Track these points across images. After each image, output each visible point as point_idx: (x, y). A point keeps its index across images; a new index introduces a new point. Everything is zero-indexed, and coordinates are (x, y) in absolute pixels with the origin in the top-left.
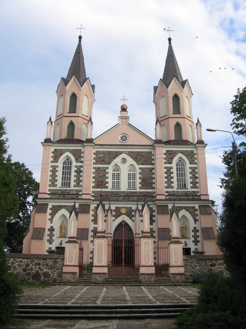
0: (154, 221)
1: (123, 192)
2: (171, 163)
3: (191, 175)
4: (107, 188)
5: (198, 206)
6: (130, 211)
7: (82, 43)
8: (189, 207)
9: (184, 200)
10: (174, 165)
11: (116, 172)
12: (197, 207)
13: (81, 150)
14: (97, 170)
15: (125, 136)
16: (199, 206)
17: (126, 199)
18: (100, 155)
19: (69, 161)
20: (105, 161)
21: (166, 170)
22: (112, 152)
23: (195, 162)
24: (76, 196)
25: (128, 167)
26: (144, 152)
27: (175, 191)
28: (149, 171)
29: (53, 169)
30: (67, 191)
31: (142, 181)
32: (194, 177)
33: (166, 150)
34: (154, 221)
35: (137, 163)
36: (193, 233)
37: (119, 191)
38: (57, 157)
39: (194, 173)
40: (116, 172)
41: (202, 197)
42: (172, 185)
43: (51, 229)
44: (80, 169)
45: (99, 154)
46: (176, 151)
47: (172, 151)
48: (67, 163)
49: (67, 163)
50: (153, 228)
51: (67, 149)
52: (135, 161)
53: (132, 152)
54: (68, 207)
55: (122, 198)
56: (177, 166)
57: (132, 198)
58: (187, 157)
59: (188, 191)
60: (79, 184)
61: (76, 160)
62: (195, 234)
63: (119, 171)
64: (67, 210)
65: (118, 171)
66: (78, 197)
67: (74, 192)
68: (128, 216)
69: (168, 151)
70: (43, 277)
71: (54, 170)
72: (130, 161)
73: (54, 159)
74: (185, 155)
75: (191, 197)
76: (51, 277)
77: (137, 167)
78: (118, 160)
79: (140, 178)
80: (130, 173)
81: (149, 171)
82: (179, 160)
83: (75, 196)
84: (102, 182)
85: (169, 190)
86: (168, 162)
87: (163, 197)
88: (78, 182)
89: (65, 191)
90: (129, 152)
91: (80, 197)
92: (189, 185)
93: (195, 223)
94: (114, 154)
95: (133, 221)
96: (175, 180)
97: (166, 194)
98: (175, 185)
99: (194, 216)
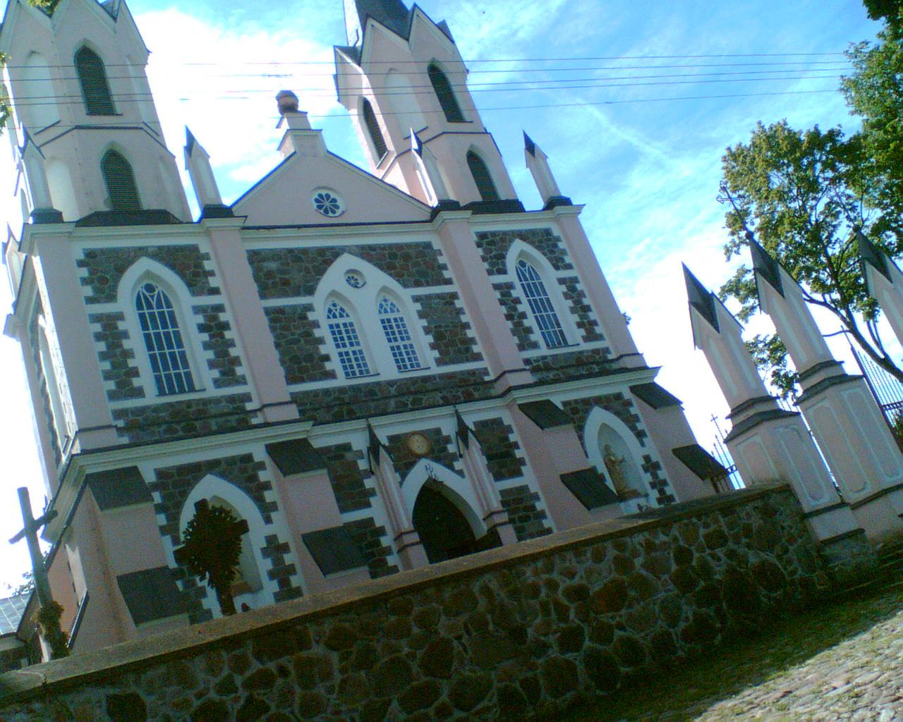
0: (274, 506)
2: (112, 298)
5: (264, 449)
6: (437, 441)
9: (571, 378)
10: (511, 277)
11: (340, 321)
12: (260, 454)
14: (275, 316)
16: (271, 449)
17: (410, 406)
18: (265, 264)
20: (292, 284)
21: (98, 327)
22: (305, 251)
23: (567, 262)
24: (237, 417)
25: (378, 295)
26: (409, 245)
27: (544, 358)
28: (445, 304)
31: (435, 338)
32: (581, 309)
34: (274, 506)
36: (649, 474)
37: (378, 384)
39: (574, 295)
40: (383, 314)
42: (136, 382)
44: (216, 318)
45: (264, 260)
46: (505, 233)
47: (494, 234)
48: (154, 303)
49: (154, 303)
54: (224, 466)
55: (422, 403)
56: (139, 306)
57: (425, 399)
58: (539, 248)
59: (581, 352)
60: (233, 372)
62: (655, 476)
63: (348, 316)
64: (222, 475)
65: (345, 315)
68: (437, 460)
69: (91, 254)
70: (764, 592)
71: (110, 331)
72: (376, 277)
73: (96, 290)
74: (532, 243)
76: (788, 578)
77: (407, 294)
78: (333, 279)
79: (427, 330)
80: (387, 317)
81: (445, 304)
82: (144, 283)
84: (310, 358)
85: (531, 354)
86: (495, 269)
88: (226, 367)
89: (184, 406)
90: (362, 247)
91: (254, 421)
92: (575, 335)
93: (268, 520)
94: (314, 260)
95: (460, 473)
96: (141, 360)
97: (121, 423)
98: (146, 379)
99: (256, 490)
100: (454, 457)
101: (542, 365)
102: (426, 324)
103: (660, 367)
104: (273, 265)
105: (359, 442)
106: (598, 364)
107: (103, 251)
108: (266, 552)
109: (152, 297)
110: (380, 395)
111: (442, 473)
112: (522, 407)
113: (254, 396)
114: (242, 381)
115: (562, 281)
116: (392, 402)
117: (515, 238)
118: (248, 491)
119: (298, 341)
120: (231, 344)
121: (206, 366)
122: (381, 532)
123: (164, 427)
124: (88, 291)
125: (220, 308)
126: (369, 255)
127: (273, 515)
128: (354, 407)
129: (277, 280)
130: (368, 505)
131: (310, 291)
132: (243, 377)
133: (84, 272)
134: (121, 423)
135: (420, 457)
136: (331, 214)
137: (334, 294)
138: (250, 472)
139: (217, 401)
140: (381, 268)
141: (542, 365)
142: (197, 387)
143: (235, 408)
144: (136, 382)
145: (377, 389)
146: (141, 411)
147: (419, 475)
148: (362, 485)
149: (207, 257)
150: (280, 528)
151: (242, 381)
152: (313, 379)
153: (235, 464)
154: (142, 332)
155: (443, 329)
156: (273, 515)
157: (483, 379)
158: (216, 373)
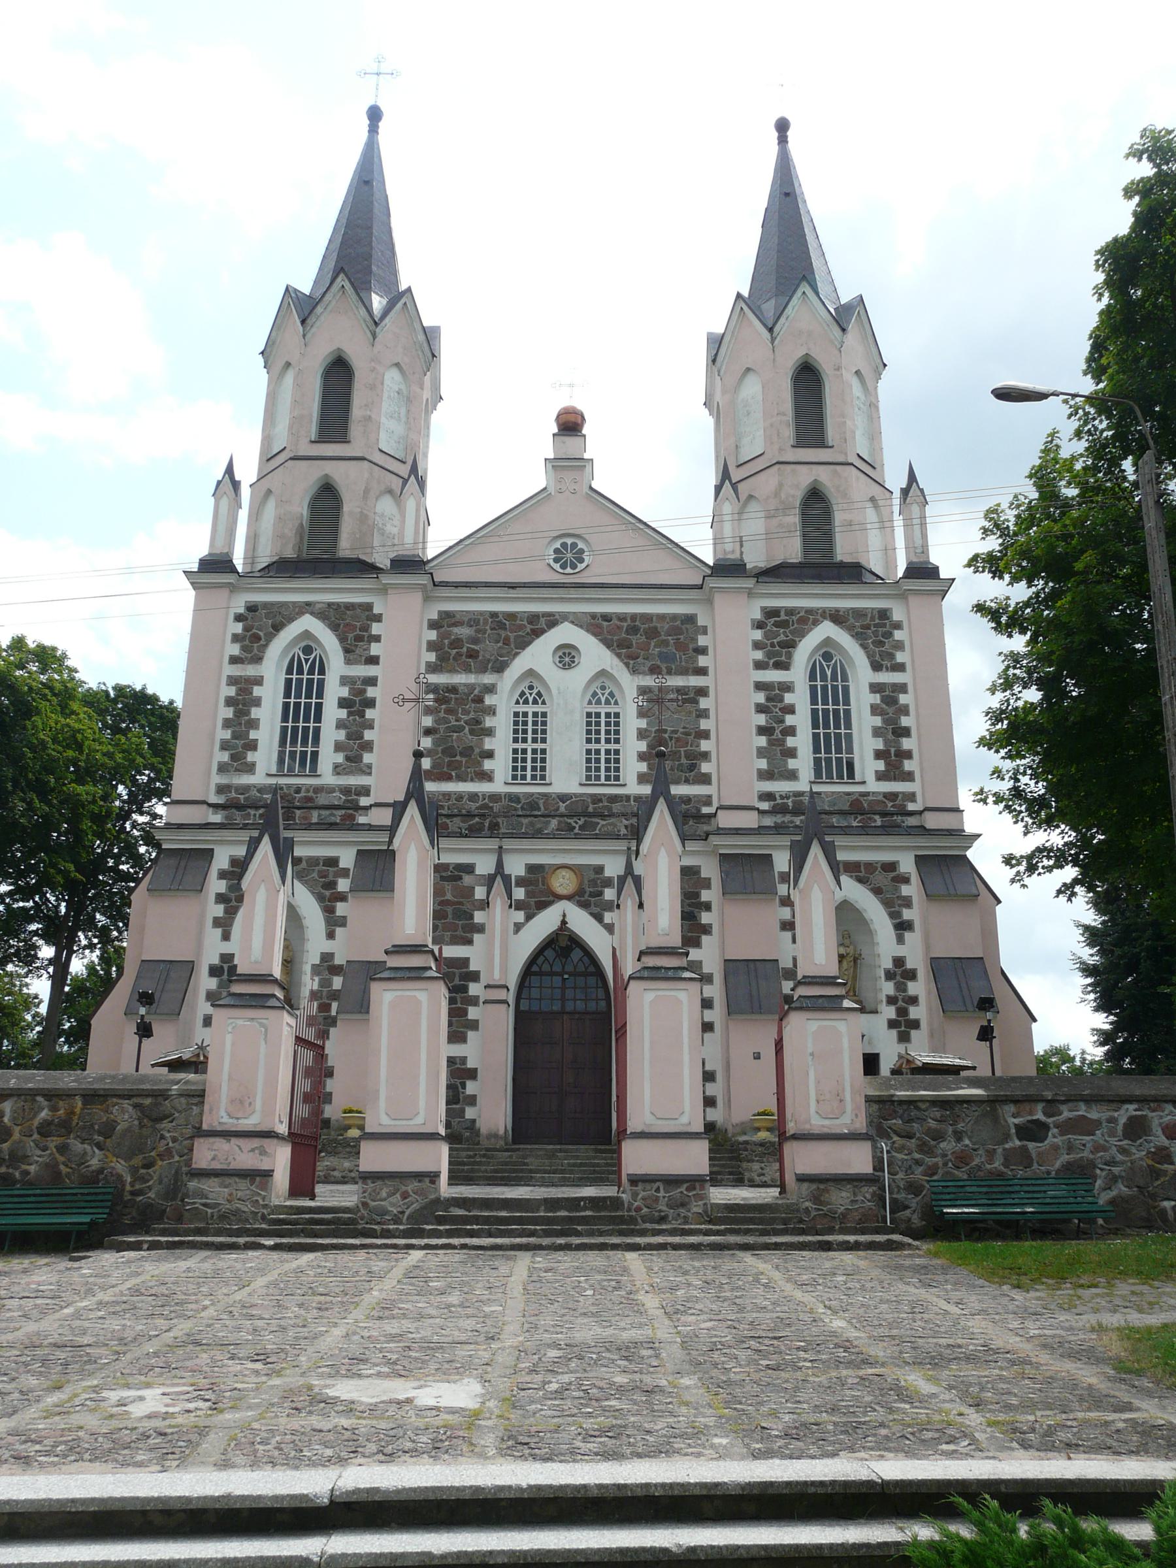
0: (342, 922)
1: (563, 798)
2: (784, 666)
3: (343, 714)
4: (487, 777)
6: (593, 882)
7: (792, 145)
8: (870, 866)
10: (798, 673)
11: (530, 709)
13: (884, 614)
15: (574, 545)
16: (920, 860)
17: (576, 831)
18: (456, 630)
19: (313, 656)
22: (512, 616)
24: (343, 812)
26: (662, 617)
29: (238, 694)
30: (303, 794)
33: (763, 609)
34: (342, 922)
35: (627, 665)
38: (260, 639)
39: (891, 710)
41: (932, 821)
43: (226, 966)
45: (455, 625)
46: (810, 611)
47: (791, 612)
48: (306, 668)
49: (306, 668)
50: (701, 962)
51: (308, 604)
52: (619, 655)
53: (606, 617)
55: (560, 822)
56: (812, 677)
59: (867, 794)
61: (347, 651)
62: (901, 987)
63: (544, 703)
66: (353, 817)
67: (337, 798)
68: (584, 905)
74: (850, 629)
75: (878, 821)
82: (821, 652)
83: (334, 812)
86: (772, 662)
87: (749, 820)
90: (593, 616)
91: (362, 820)
92: (868, 766)
93: (331, 935)
95: (610, 928)
96: (802, 741)
97: (765, 806)
98: (803, 763)
100: (610, 906)
101: (790, 804)
102: (644, 726)
103: (979, 835)
104: (464, 632)
105: (485, 865)
106: (884, 814)
107: (266, 605)
108: (316, 969)
109: (307, 660)
110: (542, 811)
111: (582, 924)
112: (724, 857)
113: (919, 798)
114: (909, 777)
115: (875, 688)
116: (554, 823)
117: (825, 618)
118: (320, 898)
119: (460, 729)
120: (370, 725)
121: (871, 755)
122: (475, 977)
123: (261, 811)
124: (235, 650)
125: (903, 688)
126: (599, 626)
127: (339, 931)
128: (500, 820)
129: (465, 649)
130: (470, 942)
131: (500, 668)
132: (369, 766)
133: (238, 628)
134: (765, 806)
135: (560, 897)
136: (569, 570)
137: (531, 673)
138: (331, 878)
139: (330, 790)
140: (608, 644)
141: (790, 804)
142: (858, 778)
143: (348, 801)
144: (792, 764)
145: (541, 802)
146: (245, 789)
147: (545, 923)
148: (472, 917)
149: (898, 626)
150: (914, 953)
151: (909, 777)
152: (461, 778)
153: (318, 865)
154: (809, 707)
155: (666, 736)
156: (339, 931)
157: (699, 810)
158: (881, 765)
